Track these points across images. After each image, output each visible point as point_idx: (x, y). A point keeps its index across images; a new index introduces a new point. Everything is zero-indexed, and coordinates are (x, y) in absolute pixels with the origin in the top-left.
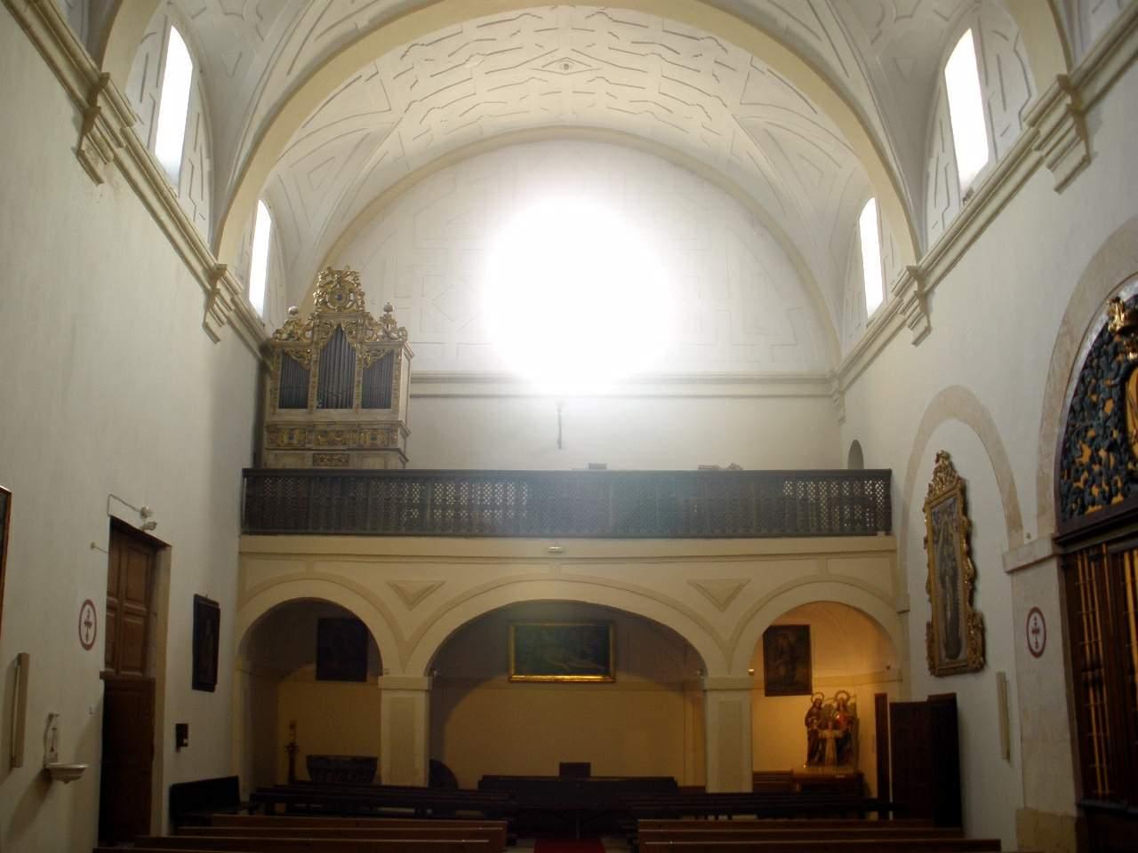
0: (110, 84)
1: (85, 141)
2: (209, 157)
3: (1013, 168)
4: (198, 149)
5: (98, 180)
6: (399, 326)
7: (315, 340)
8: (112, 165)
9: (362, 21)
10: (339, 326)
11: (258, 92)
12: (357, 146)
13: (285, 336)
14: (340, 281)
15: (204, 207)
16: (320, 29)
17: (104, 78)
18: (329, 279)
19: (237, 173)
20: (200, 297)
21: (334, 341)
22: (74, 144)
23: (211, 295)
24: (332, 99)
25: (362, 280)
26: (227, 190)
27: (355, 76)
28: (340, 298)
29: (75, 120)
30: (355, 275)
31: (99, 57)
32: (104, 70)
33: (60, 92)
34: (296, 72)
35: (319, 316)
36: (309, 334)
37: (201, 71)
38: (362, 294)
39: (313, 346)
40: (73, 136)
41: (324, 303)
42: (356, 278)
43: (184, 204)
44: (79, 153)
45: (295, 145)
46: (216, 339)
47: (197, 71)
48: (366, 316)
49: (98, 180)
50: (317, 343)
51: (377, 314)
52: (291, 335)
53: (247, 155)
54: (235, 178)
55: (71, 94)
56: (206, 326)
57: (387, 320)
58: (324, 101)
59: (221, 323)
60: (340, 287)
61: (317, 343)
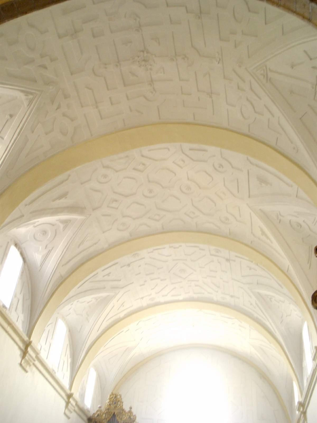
0: (32, 344)
1: (23, 361)
2: (71, 357)
3: (313, 376)
4: (66, 356)
5: (26, 371)
6: (134, 414)
7: (106, 417)
8: (32, 366)
9: (122, 315)
10: (114, 413)
11: (87, 337)
12: (125, 351)
13: (96, 415)
14: (115, 397)
15: (68, 374)
16: (108, 318)
17: (30, 343)
18: (112, 396)
19: (81, 360)
20: (63, 404)
21: (112, 419)
22: (19, 362)
23: (68, 403)
24: (113, 338)
25: (122, 397)
26: (76, 367)
27: (121, 331)
28: (115, 403)
29: (20, 355)
30: (121, 396)
31: (30, 337)
32: (31, 339)
33: (16, 347)
34: (100, 331)
35: (108, 409)
36: (104, 415)
37: (69, 331)
38: (122, 403)
39: (105, 420)
40: (19, 359)
41: (110, 405)
42: (121, 397)
43: (59, 375)
44: (21, 364)
45: (101, 352)
46: (69, 418)
47: (68, 331)
48: (123, 410)
49: (26, 371)
50: (106, 419)
51: (127, 409)
52: (98, 415)
53: (83, 357)
54: (79, 364)
55: (20, 348)
56: (65, 414)
57: (130, 412)
58: (110, 339)
59: (71, 412)
60: (115, 400)
61: (106, 419)
